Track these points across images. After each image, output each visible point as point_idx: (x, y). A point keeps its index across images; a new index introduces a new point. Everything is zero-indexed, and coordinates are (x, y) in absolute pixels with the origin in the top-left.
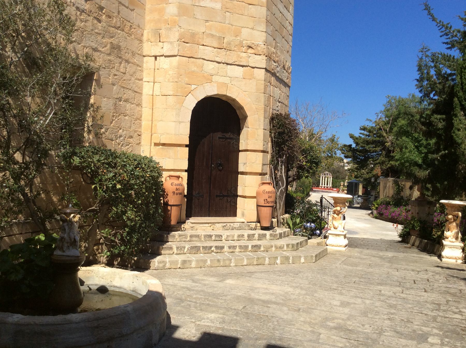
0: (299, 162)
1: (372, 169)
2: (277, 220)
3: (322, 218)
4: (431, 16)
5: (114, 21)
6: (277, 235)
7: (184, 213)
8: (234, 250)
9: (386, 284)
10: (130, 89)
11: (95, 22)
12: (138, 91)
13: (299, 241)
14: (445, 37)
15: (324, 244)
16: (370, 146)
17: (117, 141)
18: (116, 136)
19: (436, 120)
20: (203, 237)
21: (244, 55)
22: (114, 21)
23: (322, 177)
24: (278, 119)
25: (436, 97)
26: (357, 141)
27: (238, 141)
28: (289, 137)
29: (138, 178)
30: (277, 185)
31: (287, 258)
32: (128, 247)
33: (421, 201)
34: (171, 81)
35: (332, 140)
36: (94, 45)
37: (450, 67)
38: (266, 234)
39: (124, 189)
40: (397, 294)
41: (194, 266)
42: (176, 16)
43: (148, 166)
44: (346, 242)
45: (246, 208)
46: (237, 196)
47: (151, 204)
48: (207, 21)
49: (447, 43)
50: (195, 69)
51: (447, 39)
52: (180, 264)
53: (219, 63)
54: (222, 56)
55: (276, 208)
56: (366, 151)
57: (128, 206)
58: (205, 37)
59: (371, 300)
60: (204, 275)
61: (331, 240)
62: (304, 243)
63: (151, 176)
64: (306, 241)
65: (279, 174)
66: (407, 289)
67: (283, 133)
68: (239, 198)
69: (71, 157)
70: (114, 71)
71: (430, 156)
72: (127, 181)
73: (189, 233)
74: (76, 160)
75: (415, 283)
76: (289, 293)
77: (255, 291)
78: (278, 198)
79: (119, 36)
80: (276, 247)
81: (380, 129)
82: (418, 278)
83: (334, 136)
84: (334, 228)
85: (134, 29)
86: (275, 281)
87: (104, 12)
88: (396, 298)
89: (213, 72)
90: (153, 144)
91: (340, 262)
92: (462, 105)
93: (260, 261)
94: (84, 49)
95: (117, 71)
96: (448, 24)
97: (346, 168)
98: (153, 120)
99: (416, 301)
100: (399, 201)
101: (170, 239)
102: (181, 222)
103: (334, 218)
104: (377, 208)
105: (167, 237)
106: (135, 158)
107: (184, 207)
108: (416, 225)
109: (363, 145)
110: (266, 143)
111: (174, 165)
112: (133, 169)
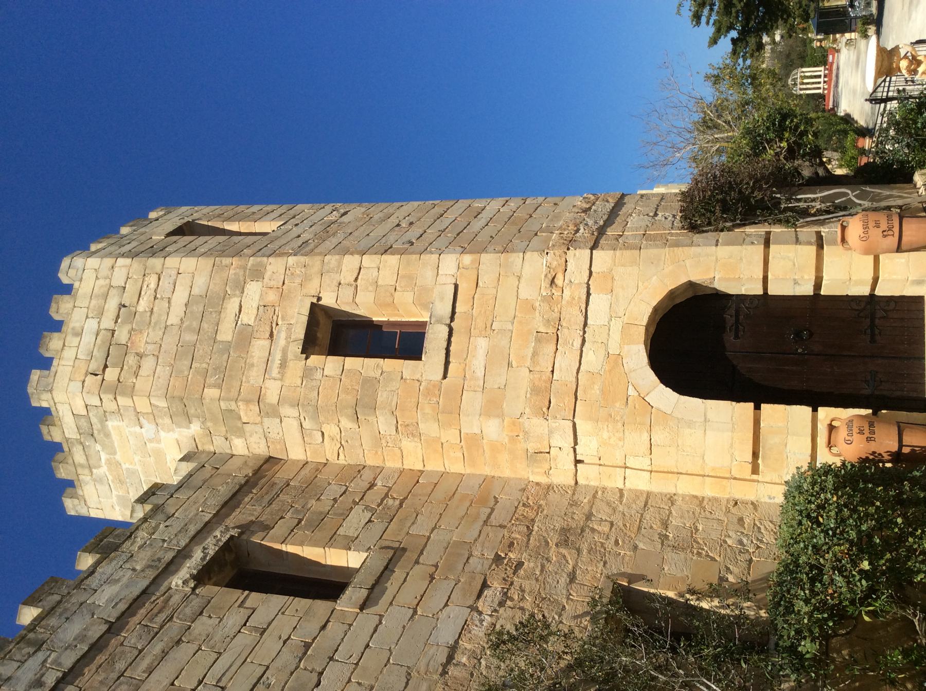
0: (782, 157)
5: (518, 536)
10: (642, 515)
11: (521, 572)
12: (643, 499)
17: (751, 551)
18: (740, 552)
22: (518, 536)
23: (801, 89)
24: (694, 216)
28: (731, 188)
29: (843, 521)
35: (717, 79)
36: (563, 580)
39: (870, 554)
43: (812, 495)
48: (509, 364)
50: (596, 387)
53: (584, 341)
55: (900, 207)
58: (538, 369)
63: (836, 489)
65: (818, 205)
67: (723, 202)
69: (801, 656)
70: (610, 544)
72: (851, 546)
74: (808, 647)
78: (875, 205)
79: (544, 529)
85: (528, 499)
87: (503, 555)
89: (602, 353)
90: (755, 477)
94: (572, 600)
95: (608, 538)
98: (701, 473)
106: (794, 523)
107: (903, 415)
109: (734, 14)
110: (748, 239)
111: (802, 438)
112: (822, 531)
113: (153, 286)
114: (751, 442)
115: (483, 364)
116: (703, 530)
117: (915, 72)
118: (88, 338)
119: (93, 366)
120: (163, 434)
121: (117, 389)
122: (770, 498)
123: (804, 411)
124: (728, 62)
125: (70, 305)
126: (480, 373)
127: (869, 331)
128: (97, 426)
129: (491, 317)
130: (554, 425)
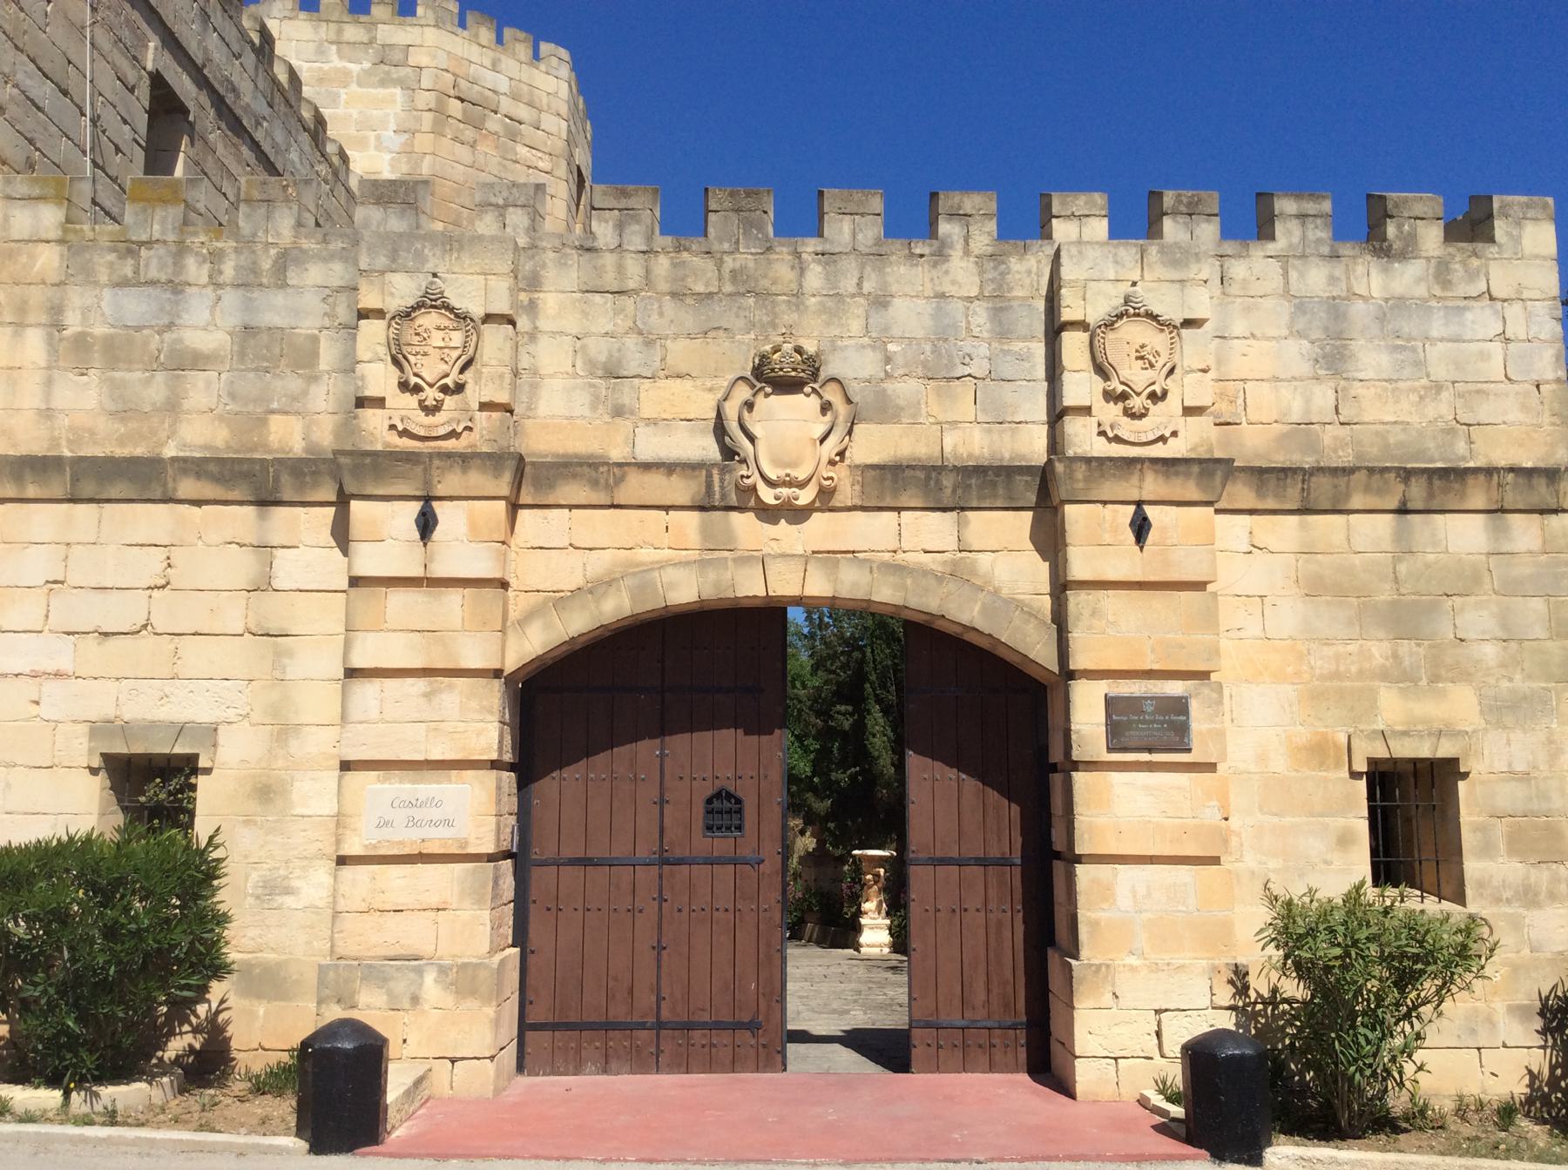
92: (876, 695)
113: (541, 165)
118: (490, 78)
119: (463, 84)
120: (387, 157)
121: (439, 111)
125: (523, 58)
128: (397, 73)
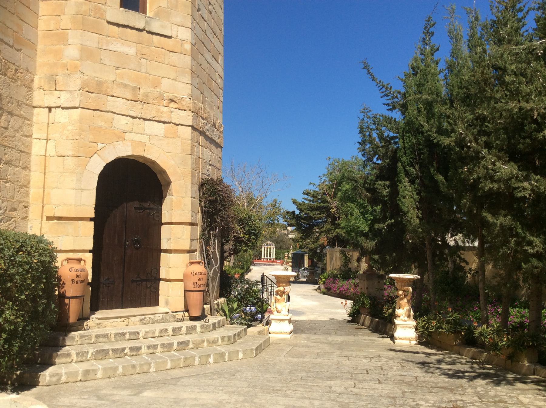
1: (318, 239)
2: (210, 307)
3: (264, 300)
4: (371, 75)
6: (209, 326)
7: (87, 306)
8: (154, 351)
9: (336, 378)
13: (236, 332)
14: (386, 98)
15: (266, 332)
16: (314, 212)
19: (380, 187)
20: (113, 336)
21: (166, 109)
24: (209, 185)
25: (379, 162)
26: (300, 207)
27: (160, 211)
29: (21, 266)
30: (209, 264)
31: (222, 355)
32: (7, 359)
33: (369, 274)
34: (70, 138)
35: (273, 205)
37: (392, 129)
38: (195, 326)
40: (349, 390)
41: (101, 377)
42: (78, 60)
43: (36, 249)
44: (291, 327)
45: (171, 295)
46: (160, 280)
47: (41, 299)
48: (117, 68)
49: (388, 105)
50: (103, 124)
51: (388, 100)
52: (80, 375)
54: (137, 110)
55: (208, 291)
56: (311, 218)
57: (6, 304)
58: (115, 86)
59: (321, 400)
60: (114, 388)
61: (274, 327)
62: (243, 333)
63: (40, 262)
64: (245, 330)
65: (211, 250)
66: (360, 381)
67: (216, 201)
68: (161, 283)
71: (377, 226)
72: (4, 270)
73: (94, 332)
75: (368, 373)
76: (224, 402)
77: (181, 404)
78: (210, 279)
80: (209, 342)
81: (324, 194)
82: (369, 365)
83: (276, 201)
84: (278, 312)
85: (21, 73)
86: (206, 388)
88: (347, 394)
89: (126, 129)
90: (45, 218)
91: (284, 354)
92: (406, 171)
93: (188, 362)
96: (388, 84)
97: (290, 236)
98: (46, 187)
99: (370, 396)
100: (347, 273)
101: (68, 343)
102: (83, 318)
103: (277, 300)
104: (324, 282)
105: (64, 339)
107: (88, 299)
108: (365, 302)
110: (194, 214)
111: (73, 246)
112: (13, 254)
114: (69, 216)
115: (118, 50)
116: (6, 187)
117: (277, 294)
122: (31, 227)
123: (90, 245)
124: (282, 211)
126: (111, 47)
127: (139, 279)
129: (149, 58)
130: (76, 94)
